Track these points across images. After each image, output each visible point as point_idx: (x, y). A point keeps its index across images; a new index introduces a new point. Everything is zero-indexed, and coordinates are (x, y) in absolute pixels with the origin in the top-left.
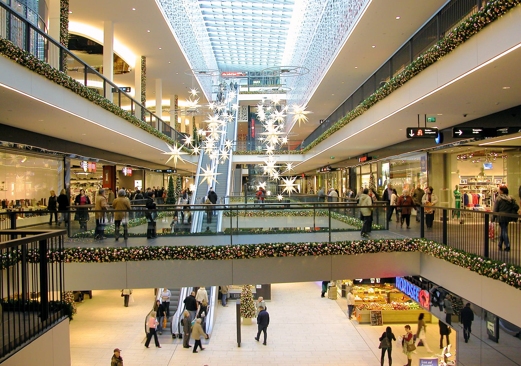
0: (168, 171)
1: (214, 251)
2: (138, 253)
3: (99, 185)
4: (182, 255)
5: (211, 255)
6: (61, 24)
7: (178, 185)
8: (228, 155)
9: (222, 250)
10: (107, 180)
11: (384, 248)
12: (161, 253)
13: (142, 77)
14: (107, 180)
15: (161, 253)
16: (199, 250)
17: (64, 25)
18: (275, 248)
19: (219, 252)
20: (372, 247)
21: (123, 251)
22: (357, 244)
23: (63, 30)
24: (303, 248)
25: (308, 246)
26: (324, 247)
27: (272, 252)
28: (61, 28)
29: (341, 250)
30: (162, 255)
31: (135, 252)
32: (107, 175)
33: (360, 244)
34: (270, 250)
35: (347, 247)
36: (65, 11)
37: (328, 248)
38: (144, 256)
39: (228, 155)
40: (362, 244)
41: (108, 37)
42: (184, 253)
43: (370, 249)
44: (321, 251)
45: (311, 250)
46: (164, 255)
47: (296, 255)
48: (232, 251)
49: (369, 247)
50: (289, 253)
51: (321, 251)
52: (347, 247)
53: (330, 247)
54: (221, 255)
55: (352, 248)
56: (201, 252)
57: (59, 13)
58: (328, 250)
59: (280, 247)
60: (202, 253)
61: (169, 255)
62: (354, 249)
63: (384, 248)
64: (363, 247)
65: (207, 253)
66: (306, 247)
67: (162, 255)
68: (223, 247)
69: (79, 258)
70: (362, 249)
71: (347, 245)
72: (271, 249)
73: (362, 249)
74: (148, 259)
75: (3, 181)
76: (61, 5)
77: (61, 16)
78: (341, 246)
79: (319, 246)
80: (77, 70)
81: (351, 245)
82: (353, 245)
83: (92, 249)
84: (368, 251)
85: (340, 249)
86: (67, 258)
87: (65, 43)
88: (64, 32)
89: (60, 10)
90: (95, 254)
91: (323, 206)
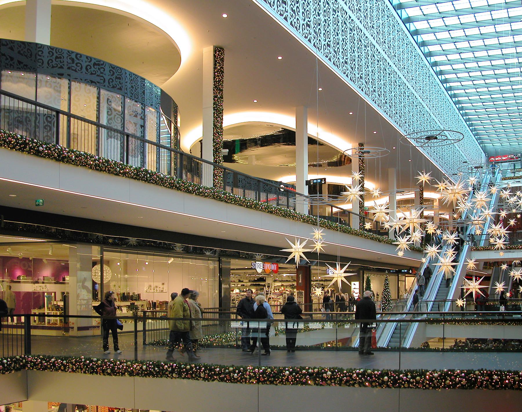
0: (403, 271)
1: (229, 373)
2: (141, 368)
3: (314, 287)
4: (191, 374)
5: (226, 377)
6: (214, 113)
7: (386, 287)
8: (500, 249)
9: (240, 372)
10: (300, 282)
11: (482, 383)
12: (167, 370)
13: (360, 167)
14: (300, 282)
15: (167, 370)
16: (211, 370)
17: (217, 114)
18: (311, 375)
19: (236, 375)
20: (460, 381)
21: (125, 364)
22: (436, 375)
23: (216, 119)
24: (351, 376)
25: (358, 374)
26: (383, 377)
27: (307, 379)
28: (214, 118)
29: (409, 382)
30: (168, 372)
31: (138, 367)
32: (300, 276)
33: (440, 376)
34: (303, 376)
35: (418, 378)
36: (219, 98)
37: (389, 378)
38: (148, 372)
39: (500, 249)
40: (445, 376)
41: (301, 122)
42: (193, 372)
43: (457, 384)
44: (378, 382)
45: (362, 380)
46: (170, 372)
47: (342, 385)
48: (252, 374)
49: (455, 381)
50: (332, 382)
51: (378, 382)
52: (418, 378)
53: (392, 378)
54: (238, 377)
55: (427, 380)
56: (213, 373)
57: (212, 101)
58: (388, 381)
59: (318, 373)
60: (215, 374)
61: (176, 373)
62: (429, 382)
63: (482, 383)
64: (446, 380)
65: (220, 374)
66: (355, 375)
67: (168, 372)
68: (242, 369)
69: (82, 369)
70: (444, 382)
71: (420, 376)
72: (305, 375)
73: (444, 382)
74: (154, 376)
75: (163, 282)
76: (214, 93)
77: (214, 104)
78: (409, 376)
79: (375, 375)
80: (320, 165)
81: (425, 377)
82: (429, 376)
83: (95, 359)
84: (454, 386)
85: (407, 381)
86: (69, 368)
87: (218, 134)
88: (218, 121)
89: (212, 98)
90: (96, 366)
91: (497, 317)
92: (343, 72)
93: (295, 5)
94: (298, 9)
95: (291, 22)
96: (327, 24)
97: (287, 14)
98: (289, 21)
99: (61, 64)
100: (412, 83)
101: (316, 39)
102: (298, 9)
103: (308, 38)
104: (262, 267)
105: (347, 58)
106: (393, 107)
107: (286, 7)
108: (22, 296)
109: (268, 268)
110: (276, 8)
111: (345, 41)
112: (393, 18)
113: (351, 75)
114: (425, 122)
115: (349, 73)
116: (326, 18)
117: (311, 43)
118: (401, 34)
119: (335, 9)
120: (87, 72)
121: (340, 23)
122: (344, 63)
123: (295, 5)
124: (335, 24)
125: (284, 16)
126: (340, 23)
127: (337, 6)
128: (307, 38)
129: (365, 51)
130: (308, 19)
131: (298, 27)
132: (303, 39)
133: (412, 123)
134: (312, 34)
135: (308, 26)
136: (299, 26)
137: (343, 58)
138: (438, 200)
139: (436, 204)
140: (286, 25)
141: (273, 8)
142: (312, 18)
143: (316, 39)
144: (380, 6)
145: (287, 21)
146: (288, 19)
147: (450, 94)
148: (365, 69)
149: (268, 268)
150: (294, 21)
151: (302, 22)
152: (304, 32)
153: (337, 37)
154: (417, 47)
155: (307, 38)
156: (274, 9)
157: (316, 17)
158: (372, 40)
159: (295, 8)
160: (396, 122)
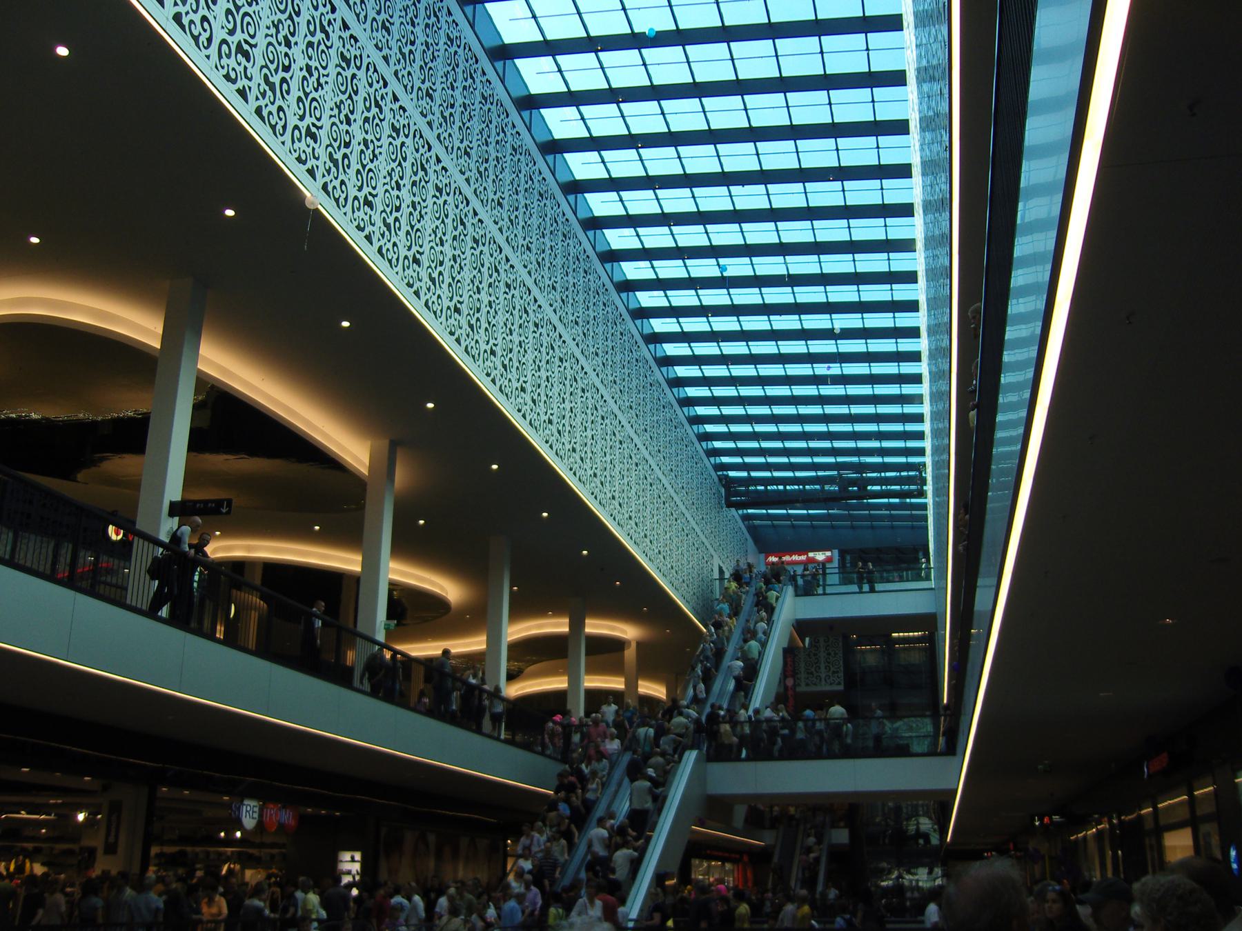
92: (485, 372)
93: (436, 268)
94: (397, 223)
95: (427, 301)
96: (458, 264)
97: (421, 284)
98: (423, 299)
100: (645, 438)
101: (385, 240)
102: (346, 161)
103: (456, 336)
104: (256, 815)
105: (526, 380)
106: (607, 484)
107: (420, 270)
108: (250, 887)
109: (271, 818)
110: (401, 272)
111: (523, 346)
112: (614, 307)
113: (531, 416)
114: (655, 501)
115: (529, 410)
116: (492, 299)
117: (419, 298)
118: (610, 311)
119: (509, 282)
121: (517, 310)
122: (547, 422)
123: (436, 268)
124: (507, 312)
125: (415, 288)
126: (517, 310)
127: (513, 277)
128: (304, 163)
129: (536, 335)
130: (459, 298)
131: (477, 356)
132: (352, 229)
133: (626, 500)
134: (498, 369)
135: (457, 310)
136: (479, 354)
137: (519, 380)
138: (634, 645)
139: (630, 654)
140: (367, 254)
141: (344, 210)
142: (466, 297)
143: (385, 240)
144: (548, 209)
145: (460, 344)
146: (422, 295)
147: (705, 447)
148: (581, 433)
149: (271, 818)
150: (387, 246)
151: (446, 303)
152: (485, 366)
153: (510, 337)
154: (655, 368)
155: (304, 163)
156: (397, 273)
157: (506, 337)
158: (575, 349)
159: (473, 322)
160: (592, 494)
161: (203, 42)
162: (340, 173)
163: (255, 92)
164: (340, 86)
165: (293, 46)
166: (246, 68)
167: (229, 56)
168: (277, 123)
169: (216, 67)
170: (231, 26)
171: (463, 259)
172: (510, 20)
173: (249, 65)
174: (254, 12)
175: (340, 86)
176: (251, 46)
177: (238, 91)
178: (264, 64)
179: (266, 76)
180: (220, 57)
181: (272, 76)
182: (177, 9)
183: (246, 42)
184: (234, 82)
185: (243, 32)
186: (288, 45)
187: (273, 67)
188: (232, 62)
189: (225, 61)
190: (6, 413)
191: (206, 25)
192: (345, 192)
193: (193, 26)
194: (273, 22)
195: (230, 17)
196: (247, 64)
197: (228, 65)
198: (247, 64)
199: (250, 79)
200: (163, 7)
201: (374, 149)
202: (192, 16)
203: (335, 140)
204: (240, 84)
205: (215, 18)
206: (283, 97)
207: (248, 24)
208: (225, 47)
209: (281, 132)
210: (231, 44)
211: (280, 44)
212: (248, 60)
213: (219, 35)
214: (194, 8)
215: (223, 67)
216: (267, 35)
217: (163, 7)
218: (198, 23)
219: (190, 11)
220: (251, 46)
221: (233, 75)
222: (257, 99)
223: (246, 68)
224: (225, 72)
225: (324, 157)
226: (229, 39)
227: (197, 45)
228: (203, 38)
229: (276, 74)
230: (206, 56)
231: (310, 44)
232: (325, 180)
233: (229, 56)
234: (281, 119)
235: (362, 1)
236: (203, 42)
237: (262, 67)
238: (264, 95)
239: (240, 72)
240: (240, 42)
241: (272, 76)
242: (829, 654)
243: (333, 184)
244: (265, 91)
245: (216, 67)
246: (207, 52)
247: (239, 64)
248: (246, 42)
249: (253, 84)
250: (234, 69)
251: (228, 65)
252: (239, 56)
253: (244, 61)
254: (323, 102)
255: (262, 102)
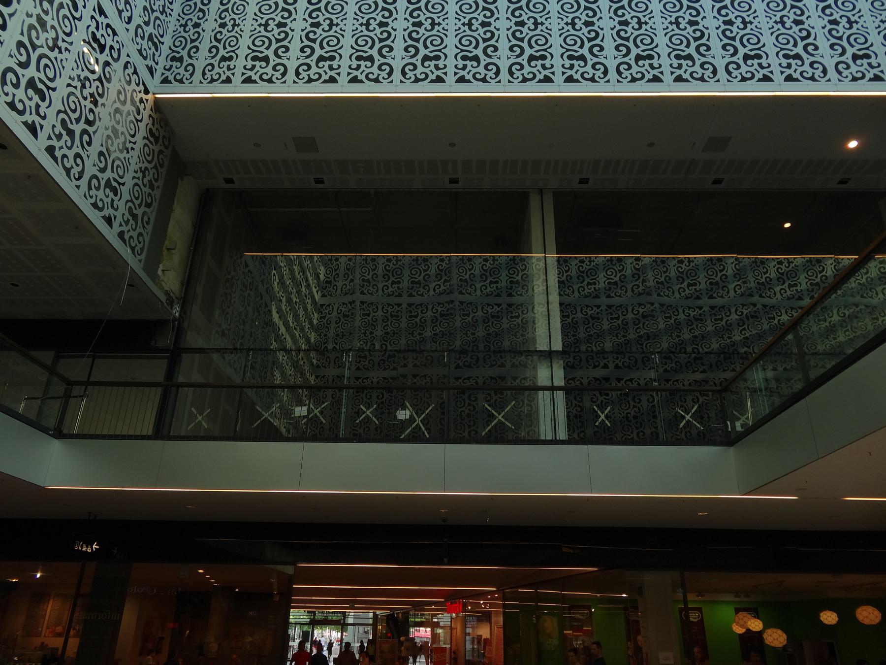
99: (229, 73)
101: (129, 227)
120: (511, 79)
143: (129, 227)
161: (74, 174)
162: (138, 226)
163: (47, 130)
164: (146, 156)
165: (155, 189)
166: (113, 201)
167: (98, 189)
168: (136, 245)
169: (85, 196)
170: (102, 165)
171: (234, 298)
172: (285, 144)
173: (116, 199)
174: (125, 158)
175: (146, 156)
176: (119, 184)
177: (104, 217)
178: (130, 199)
179: (130, 208)
180: (90, 188)
181: (136, 209)
182: (50, 143)
183: (115, 180)
184: (101, 210)
185: (113, 172)
186: (95, 103)
187: (137, 202)
188: (100, 194)
189: (93, 192)
190: (334, 616)
191: (79, 161)
192: (142, 242)
193: (132, 240)
194: (140, 168)
195: (102, 158)
196: (114, 198)
197: (96, 196)
198: (114, 198)
199: (116, 210)
200: (37, 139)
201: (231, 300)
202: (132, 233)
203: (137, 199)
204: (106, 212)
205: (88, 157)
206: (144, 227)
207: (46, 66)
208: (94, 181)
209: (139, 253)
210: (101, 179)
211: (145, 186)
212: (116, 195)
213: (90, 170)
214: (134, 227)
215: (91, 197)
216: (134, 178)
217: (37, 139)
218: (136, 238)
219: (131, 230)
220: (119, 184)
221: (100, 204)
222: (121, 225)
223: (113, 201)
224: (93, 201)
225: (122, 209)
226: (100, 175)
227: (68, 175)
228: (75, 171)
229: (139, 208)
230: (76, 186)
231: (117, 111)
232: (121, 229)
233: (98, 189)
234: (140, 243)
235: (127, 2)
236: (74, 174)
237: (127, 201)
238: (127, 222)
239: (107, 203)
240: (109, 178)
241: (136, 209)
242: (325, 335)
243: (130, 234)
244: (128, 220)
245: (85, 196)
246: (78, 183)
247: (107, 197)
248: (115, 180)
249: (119, 214)
250: (101, 200)
251: (96, 196)
252: (108, 190)
253: (111, 195)
254: (128, 164)
255: (124, 228)
